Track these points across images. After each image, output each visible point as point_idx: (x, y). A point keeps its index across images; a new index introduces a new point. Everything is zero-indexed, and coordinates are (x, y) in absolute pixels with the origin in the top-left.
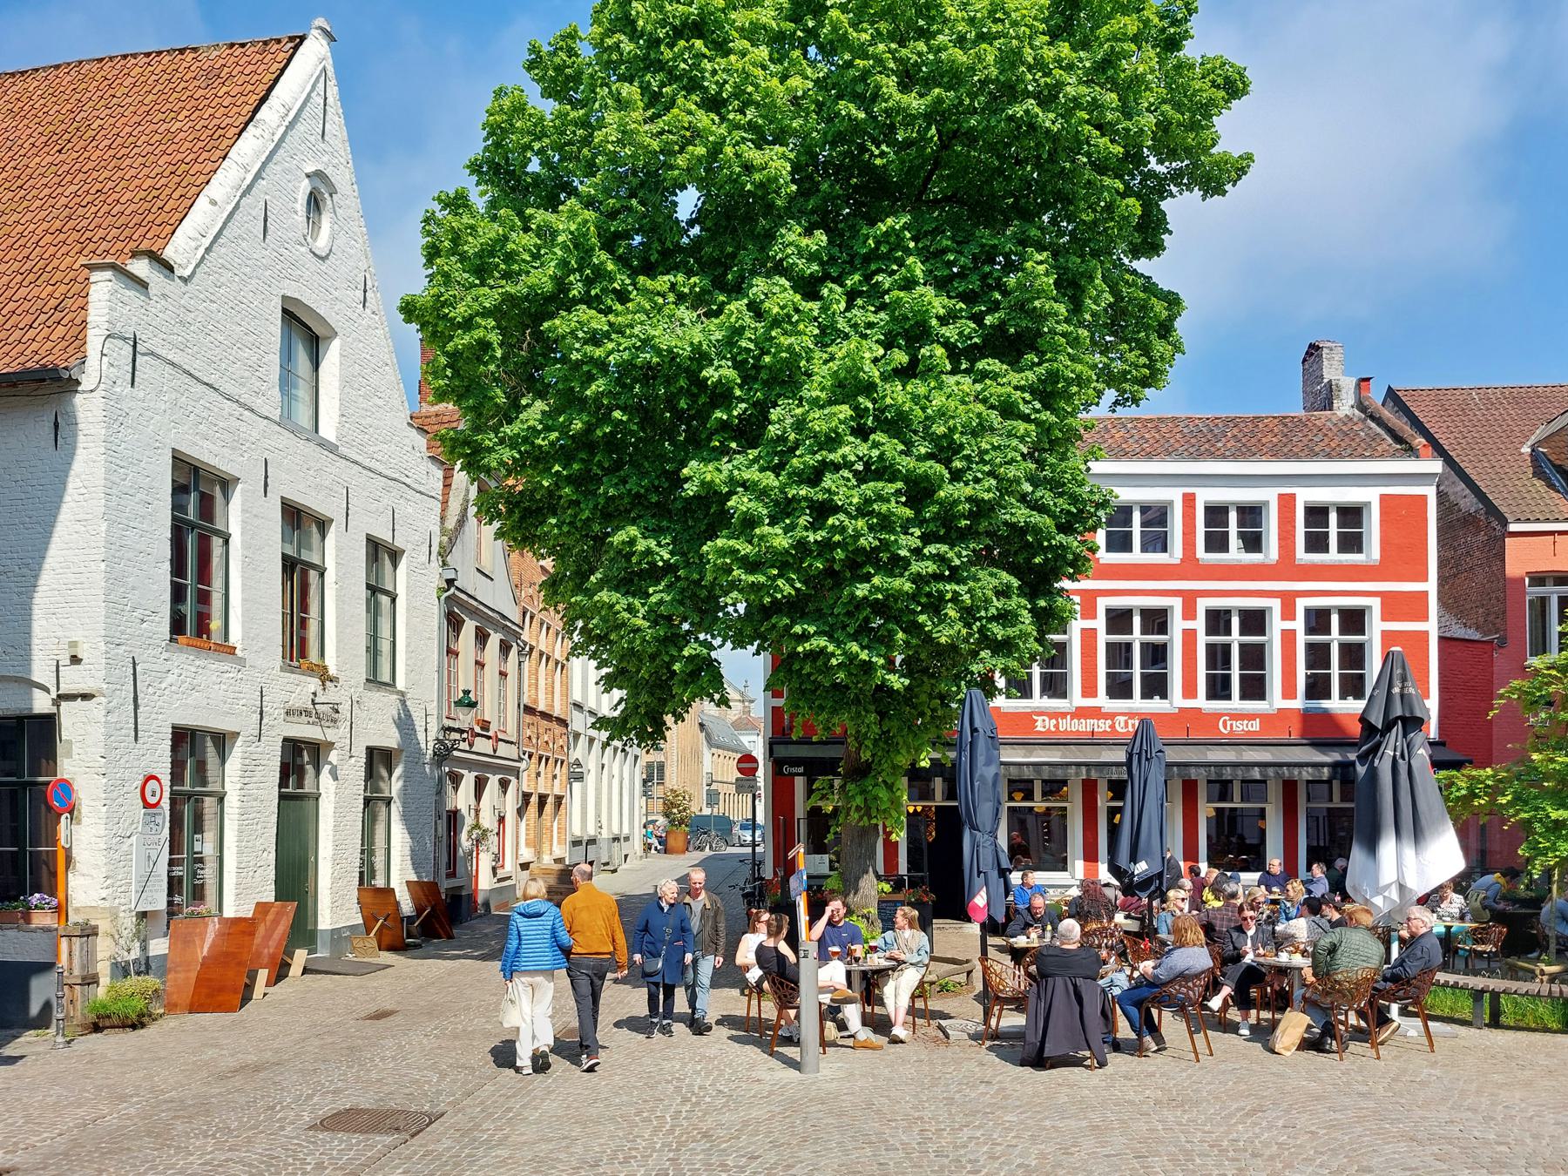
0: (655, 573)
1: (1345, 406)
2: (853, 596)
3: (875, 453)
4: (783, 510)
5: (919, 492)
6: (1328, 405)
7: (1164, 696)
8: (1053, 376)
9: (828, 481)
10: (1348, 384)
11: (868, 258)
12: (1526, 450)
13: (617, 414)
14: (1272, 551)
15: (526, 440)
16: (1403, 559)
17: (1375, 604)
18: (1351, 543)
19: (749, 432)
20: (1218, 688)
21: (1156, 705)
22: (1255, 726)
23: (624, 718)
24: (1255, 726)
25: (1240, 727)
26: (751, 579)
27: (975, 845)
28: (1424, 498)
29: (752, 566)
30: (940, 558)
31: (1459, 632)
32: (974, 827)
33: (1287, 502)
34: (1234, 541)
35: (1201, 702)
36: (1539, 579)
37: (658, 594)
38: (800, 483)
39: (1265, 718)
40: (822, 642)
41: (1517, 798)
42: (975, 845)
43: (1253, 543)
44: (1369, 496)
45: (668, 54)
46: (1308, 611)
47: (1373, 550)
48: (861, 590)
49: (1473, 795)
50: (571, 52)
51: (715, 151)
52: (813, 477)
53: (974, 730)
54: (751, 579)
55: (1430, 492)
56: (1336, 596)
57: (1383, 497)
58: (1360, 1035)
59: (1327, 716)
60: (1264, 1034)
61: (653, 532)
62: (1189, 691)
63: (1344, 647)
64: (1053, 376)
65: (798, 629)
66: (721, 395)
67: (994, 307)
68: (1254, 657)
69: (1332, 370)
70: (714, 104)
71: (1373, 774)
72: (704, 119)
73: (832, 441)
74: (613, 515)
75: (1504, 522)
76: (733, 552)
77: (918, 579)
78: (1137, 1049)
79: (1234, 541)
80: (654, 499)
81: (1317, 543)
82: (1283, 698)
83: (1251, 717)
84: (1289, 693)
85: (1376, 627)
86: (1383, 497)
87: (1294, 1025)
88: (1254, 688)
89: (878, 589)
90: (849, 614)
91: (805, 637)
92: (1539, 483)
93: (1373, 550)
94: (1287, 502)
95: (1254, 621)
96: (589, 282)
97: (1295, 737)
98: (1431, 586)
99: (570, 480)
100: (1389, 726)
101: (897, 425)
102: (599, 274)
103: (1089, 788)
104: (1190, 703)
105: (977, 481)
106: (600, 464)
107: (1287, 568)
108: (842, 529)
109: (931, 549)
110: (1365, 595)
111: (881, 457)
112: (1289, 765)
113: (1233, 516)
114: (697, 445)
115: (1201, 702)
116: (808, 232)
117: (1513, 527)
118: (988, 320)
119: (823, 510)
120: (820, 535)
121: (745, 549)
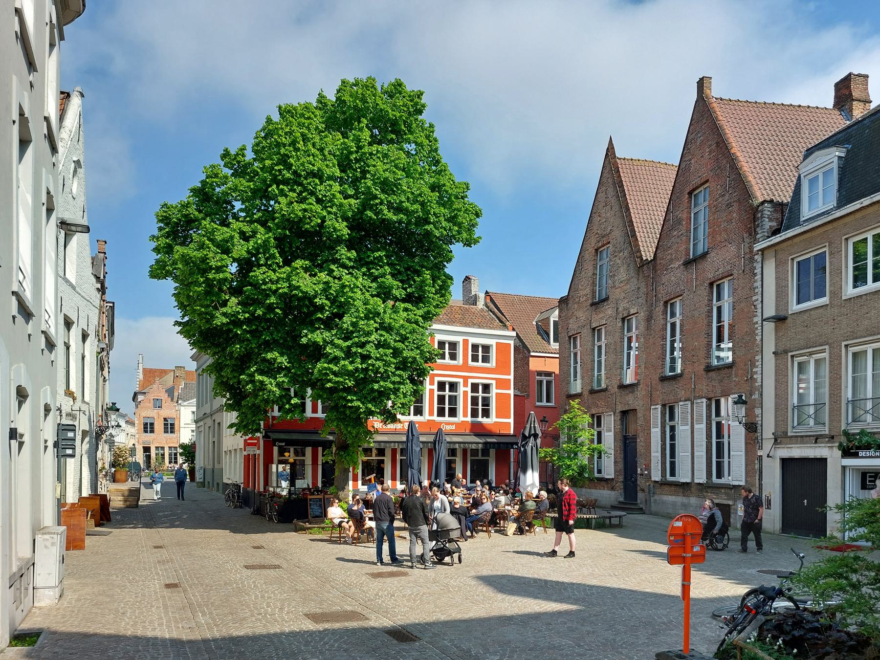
0: (280, 369)
1: (481, 304)
2: (372, 388)
3: (383, 339)
4: (349, 354)
5: (396, 353)
6: (475, 303)
7: (421, 415)
8: (429, 312)
9: (368, 347)
10: (482, 296)
11: (372, 262)
12: (534, 323)
13: (278, 311)
14: (460, 361)
15: (233, 315)
16: (502, 367)
17: (494, 382)
18: (486, 359)
19: (328, 324)
20: (441, 413)
21: (418, 418)
22: (453, 427)
23: (242, 421)
24: (453, 427)
25: (449, 427)
26: (337, 379)
27: (412, 475)
28: (510, 344)
29: (335, 374)
30: (400, 376)
31: (518, 393)
32: (412, 468)
33: (466, 342)
34: (447, 356)
35: (435, 418)
36: (540, 374)
37: (281, 378)
38: (357, 347)
39: (456, 424)
40: (359, 403)
41: (559, 458)
42: (412, 475)
43: (453, 357)
44: (492, 342)
45: (305, 182)
46: (472, 384)
47: (493, 364)
48: (376, 386)
49: (546, 457)
50: (243, 156)
51: (323, 221)
52: (363, 345)
53: (413, 435)
54: (337, 379)
55: (512, 342)
56: (481, 379)
57: (497, 343)
58: (527, 531)
59: (480, 424)
60: (502, 532)
61: (282, 354)
62: (431, 414)
63: (483, 398)
64: (429, 312)
65: (349, 397)
66: (321, 308)
67: (410, 286)
68: (453, 400)
69: (475, 289)
70: (319, 201)
71: (525, 450)
72: (318, 208)
73: (368, 334)
74: (268, 346)
75: (529, 352)
76: (330, 369)
77: (394, 383)
78: (472, 537)
79: (447, 356)
80: (281, 341)
81: (475, 359)
82: (463, 417)
83: (452, 424)
84: (465, 415)
85: (494, 391)
86: (497, 343)
87: (512, 527)
88: (453, 412)
89: (382, 386)
90: (369, 394)
91: (352, 401)
92: (539, 337)
93: (493, 364)
94: (466, 342)
95: (453, 386)
96: (267, 259)
97: (468, 432)
98: (511, 377)
99: (248, 332)
100: (530, 437)
101: (389, 329)
102: (273, 256)
103: (394, 451)
104: (431, 418)
105: (412, 350)
106: (263, 327)
107: (465, 367)
108: (373, 365)
109: (398, 372)
110: (490, 379)
111: (385, 340)
112: (468, 443)
113: (447, 346)
114: (312, 326)
115: (435, 418)
116: (349, 250)
117: (532, 354)
118: (408, 290)
119: (365, 358)
120: (364, 366)
121: (335, 369)
